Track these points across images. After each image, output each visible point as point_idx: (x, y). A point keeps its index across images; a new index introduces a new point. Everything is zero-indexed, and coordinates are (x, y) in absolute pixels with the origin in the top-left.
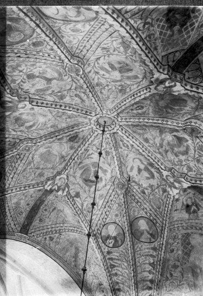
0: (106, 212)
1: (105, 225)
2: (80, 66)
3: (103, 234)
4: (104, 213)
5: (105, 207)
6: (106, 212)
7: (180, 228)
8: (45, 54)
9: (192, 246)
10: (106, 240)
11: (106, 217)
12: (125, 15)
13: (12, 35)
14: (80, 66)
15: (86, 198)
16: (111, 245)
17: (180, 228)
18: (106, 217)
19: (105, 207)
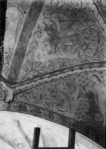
0: (14, 134)
1: (15, 139)
2: (23, 103)
3: (16, 143)
4: (13, 135)
5: (12, 132)
6: (14, 134)
7: (49, 136)
8: (75, 31)
9: (57, 142)
10: (18, 145)
11: (15, 136)
12: (63, 10)
13: (94, 92)
14: (23, 103)
15: (2, 130)
16: (21, 147)
17: (49, 136)
18: (15, 136)
19: (12, 132)
